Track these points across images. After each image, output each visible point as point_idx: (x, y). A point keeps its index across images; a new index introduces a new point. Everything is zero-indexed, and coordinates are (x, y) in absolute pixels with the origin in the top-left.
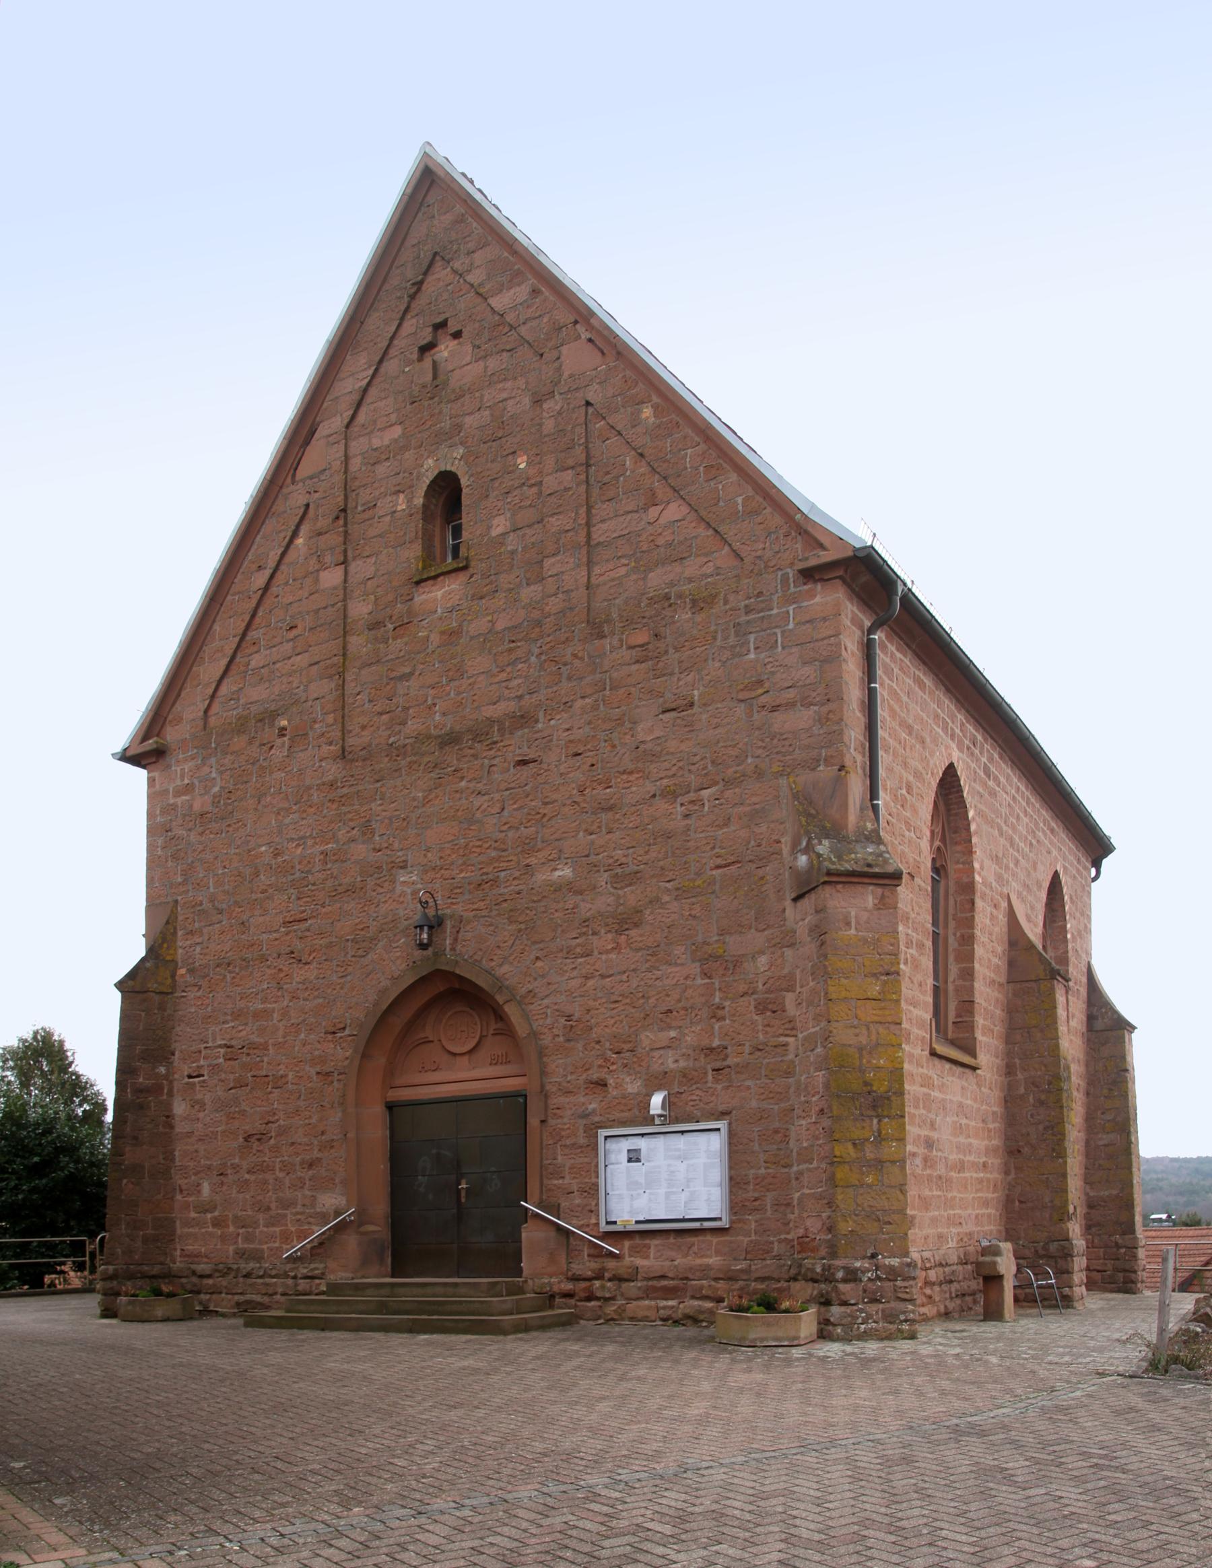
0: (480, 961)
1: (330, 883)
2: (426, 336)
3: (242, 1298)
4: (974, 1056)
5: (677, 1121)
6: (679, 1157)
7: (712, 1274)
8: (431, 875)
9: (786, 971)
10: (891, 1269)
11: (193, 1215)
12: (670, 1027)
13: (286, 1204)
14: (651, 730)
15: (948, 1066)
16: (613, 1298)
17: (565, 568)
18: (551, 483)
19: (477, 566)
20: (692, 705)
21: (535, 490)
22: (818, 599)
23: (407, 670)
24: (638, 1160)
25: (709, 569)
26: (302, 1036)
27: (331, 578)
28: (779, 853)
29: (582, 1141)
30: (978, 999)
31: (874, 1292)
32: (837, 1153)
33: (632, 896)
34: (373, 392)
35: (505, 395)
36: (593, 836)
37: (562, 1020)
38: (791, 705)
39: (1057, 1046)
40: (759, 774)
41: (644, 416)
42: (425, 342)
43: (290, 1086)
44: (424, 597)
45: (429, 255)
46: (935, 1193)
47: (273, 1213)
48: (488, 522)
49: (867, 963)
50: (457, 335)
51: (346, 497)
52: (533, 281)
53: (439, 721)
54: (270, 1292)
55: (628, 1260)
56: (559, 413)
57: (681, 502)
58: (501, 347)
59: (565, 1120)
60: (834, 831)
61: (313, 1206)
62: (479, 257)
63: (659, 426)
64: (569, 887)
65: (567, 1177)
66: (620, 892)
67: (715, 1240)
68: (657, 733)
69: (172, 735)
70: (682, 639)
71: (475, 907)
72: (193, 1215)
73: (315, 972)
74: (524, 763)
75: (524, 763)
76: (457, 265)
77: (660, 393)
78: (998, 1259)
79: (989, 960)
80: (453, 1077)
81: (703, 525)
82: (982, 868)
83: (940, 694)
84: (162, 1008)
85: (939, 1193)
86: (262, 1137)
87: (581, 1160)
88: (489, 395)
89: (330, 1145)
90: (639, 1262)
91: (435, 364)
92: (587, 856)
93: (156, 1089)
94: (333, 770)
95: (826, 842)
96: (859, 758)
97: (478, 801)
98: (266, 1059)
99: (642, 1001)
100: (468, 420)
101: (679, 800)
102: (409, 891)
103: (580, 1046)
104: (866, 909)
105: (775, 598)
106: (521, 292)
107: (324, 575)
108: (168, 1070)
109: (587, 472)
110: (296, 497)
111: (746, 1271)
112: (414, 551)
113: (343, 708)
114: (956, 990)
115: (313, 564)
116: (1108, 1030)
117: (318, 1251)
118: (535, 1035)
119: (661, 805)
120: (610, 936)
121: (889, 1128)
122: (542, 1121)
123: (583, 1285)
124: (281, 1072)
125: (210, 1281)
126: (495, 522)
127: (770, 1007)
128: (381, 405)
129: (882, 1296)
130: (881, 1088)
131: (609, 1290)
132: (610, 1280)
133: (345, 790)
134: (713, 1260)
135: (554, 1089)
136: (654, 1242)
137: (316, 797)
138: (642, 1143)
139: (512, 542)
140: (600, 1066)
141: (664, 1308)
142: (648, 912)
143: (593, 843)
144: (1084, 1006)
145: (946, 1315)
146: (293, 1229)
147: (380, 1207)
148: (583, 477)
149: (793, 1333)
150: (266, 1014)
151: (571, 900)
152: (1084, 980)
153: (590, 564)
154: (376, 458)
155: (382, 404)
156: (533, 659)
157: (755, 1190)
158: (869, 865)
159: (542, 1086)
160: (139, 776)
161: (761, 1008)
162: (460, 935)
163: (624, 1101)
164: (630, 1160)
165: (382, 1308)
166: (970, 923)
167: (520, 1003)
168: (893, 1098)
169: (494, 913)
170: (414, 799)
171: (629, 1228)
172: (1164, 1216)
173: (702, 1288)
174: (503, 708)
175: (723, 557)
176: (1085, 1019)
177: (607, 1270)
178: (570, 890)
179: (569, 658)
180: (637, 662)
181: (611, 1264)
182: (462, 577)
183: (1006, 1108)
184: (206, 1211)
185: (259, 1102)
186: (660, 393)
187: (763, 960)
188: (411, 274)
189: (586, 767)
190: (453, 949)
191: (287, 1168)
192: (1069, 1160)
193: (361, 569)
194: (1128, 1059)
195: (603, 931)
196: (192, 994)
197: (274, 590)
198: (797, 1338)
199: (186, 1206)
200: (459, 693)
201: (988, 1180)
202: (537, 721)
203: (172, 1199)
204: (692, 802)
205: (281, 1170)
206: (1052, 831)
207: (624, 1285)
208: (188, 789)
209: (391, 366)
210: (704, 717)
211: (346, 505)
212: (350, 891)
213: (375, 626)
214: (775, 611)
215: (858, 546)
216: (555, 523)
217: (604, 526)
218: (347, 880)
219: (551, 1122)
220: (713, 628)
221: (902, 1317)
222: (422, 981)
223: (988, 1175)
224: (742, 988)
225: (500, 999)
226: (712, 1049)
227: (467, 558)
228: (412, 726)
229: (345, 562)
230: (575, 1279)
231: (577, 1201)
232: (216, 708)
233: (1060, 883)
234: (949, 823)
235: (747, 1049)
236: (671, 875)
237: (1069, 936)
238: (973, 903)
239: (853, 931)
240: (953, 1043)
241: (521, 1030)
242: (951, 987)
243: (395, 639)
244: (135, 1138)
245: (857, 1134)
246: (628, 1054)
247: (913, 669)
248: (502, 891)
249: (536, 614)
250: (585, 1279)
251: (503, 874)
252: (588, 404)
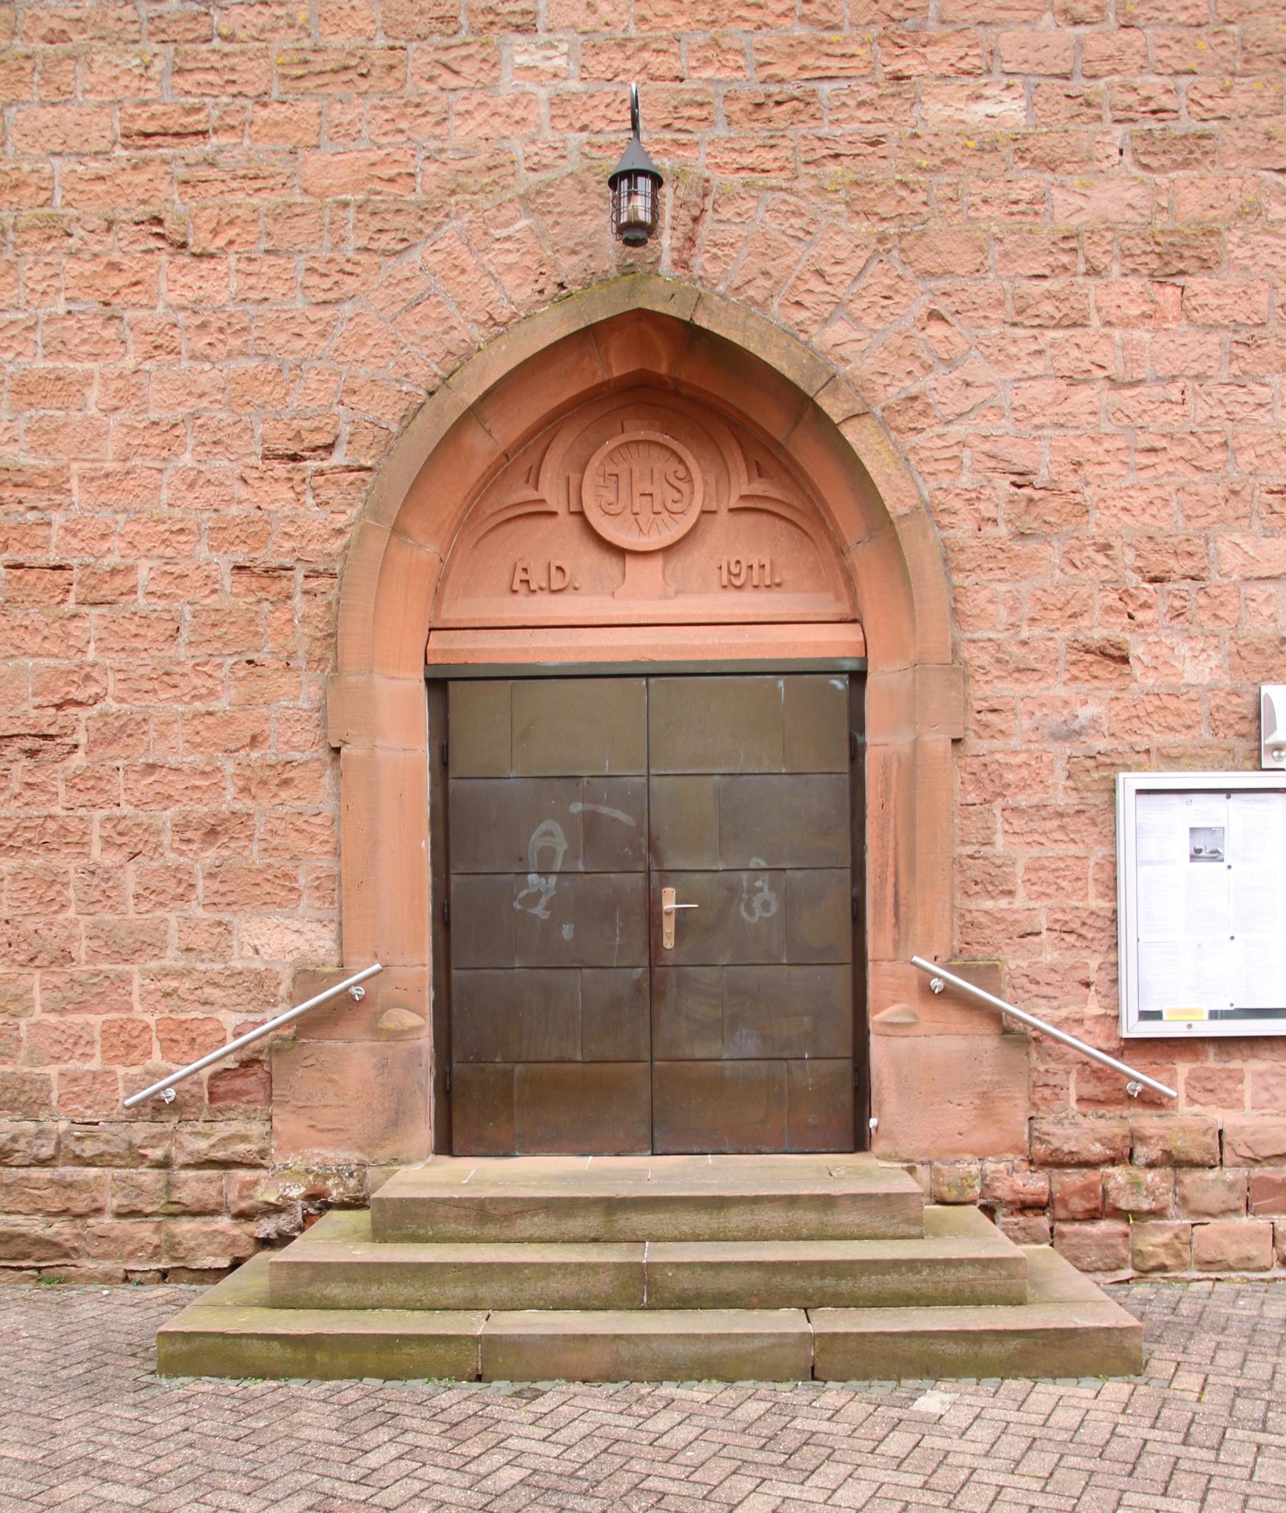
0: (763, 305)
1: (283, 41)
24: (1215, 856)
26: (187, 459)
33: (1192, 195)
36: (1081, 30)
37: (1004, 483)
43: (142, 602)
47: (80, 969)
54: (80, 1207)
59: (1014, 743)
61: (220, 952)
65: (1021, 892)
66: (1159, 178)
71: (746, 160)
73: (235, 283)
87: (1061, 849)
89: (282, 777)
92: (1066, 77)
98: (58, 518)
99: (1219, 456)
102: (543, 94)
103: (1053, 553)
117: (238, 1084)
120: (1135, 284)
122: (956, 742)
123: (1074, 1178)
124: (112, 560)
131: (1151, 1192)
132: (1151, 1165)
135: (985, 660)
136: (1254, 1066)
140: (1109, 610)
142: (1234, 237)
143: (1080, 45)
146: (151, 1020)
151: (1028, 182)
162: (704, 230)
163: (1173, 704)
164: (1196, 855)
167: (884, 424)
169: (803, 185)
177: (1143, 1140)
178: (1021, 154)
185: (33, 643)
191: (129, 840)
195: (1116, 269)
205: (108, 842)
207: (1191, 1178)
212: (352, 69)
219: (975, 745)
222: (588, 338)
225: (834, 408)
230: (1056, 1162)
231: (1050, 957)
241: (895, 499)
246: (1185, 584)
251: (826, 88)
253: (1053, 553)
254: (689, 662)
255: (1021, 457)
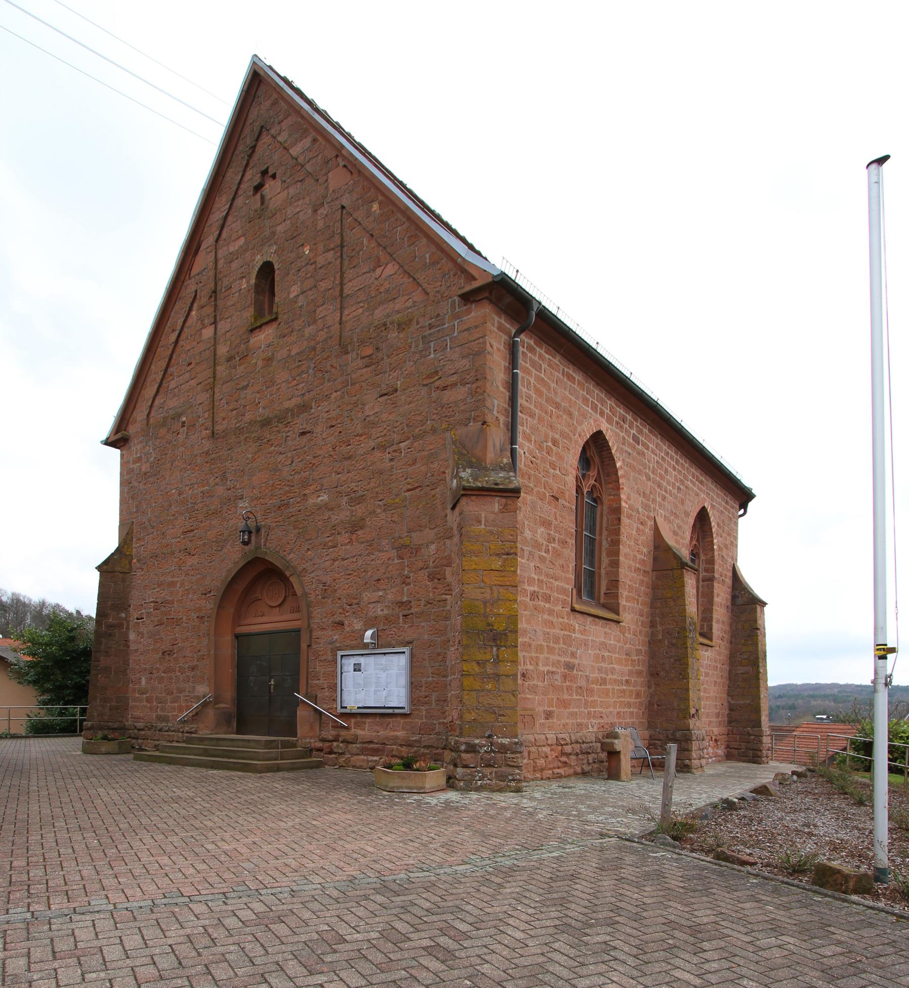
1: (205, 509)
2: (257, 180)
3: (157, 742)
4: (618, 614)
5: (382, 647)
6: (382, 669)
7: (399, 742)
8: (255, 502)
9: (446, 554)
10: (502, 745)
11: (137, 695)
12: (379, 590)
13: (180, 691)
14: (373, 408)
15: (590, 619)
16: (343, 753)
17: (328, 313)
18: (321, 260)
19: (282, 318)
20: (396, 390)
21: (313, 266)
22: (473, 314)
23: (245, 384)
24: (360, 670)
25: (409, 304)
27: (208, 332)
28: (444, 480)
29: (330, 658)
30: (622, 578)
31: (489, 760)
32: (465, 669)
33: (360, 510)
34: (230, 218)
35: (298, 210)
37: (321, 586)
38: (454, 385)
39: (685, 610)
40: (434, 430)
41: (374, 209)
42: (256, 184)
44: (255, 339)
45: (259, 128)
46: (575, 697)
48: (289, 290)
49: (492, 547)
50: (274, 177)
51: (216, 284)
52: (313, 134)
53: (262, 412)
55: (353, 731)
56: (326, 216)
57: (394, 262)
58: (297, 179)
60: (478, 465)
62: (284, 125)
63: (382, 215)
64: (327, 507)
66: (354, 508)
67: (402, 721)
68: (377, 410)
69: (132, 430)
70: (391, 350)
72: (137, 695)
74: (303, 434)
75: (303, 434)
76: (273, 132)
77: (383, 194)
78: (616, 741)
79: (635, 556)
80: (273, 619)
81: (407, 275)
82: (629, 498)
83: (591, 386)
84: (124, 581)
85: (579, 697)
86: (170, 653)
88: (290, 211)
90: (360, 732)
91: (262, 197)
93: (120, 626)
94: (207, 445)
95: (469, 471)
96: (502, 419)
97: (280, 458)
100: (279, 228)
101: (388, 450)
103: (329, 601)
104: (493, 512)
105: (447, 317)
106: (307, 142)
107: (204, 331)
108: (126, 615)
109: (342, 251)
110: (190, 287)
111: (419, 741)
112: (249, 313)
113: (213, 408)
114: (607, 574)
115: (199, 325)
116: (746, 606)
118: (306, 594)
119: (378, 454)
121: (505, 653)
123: (328, 744)
125: (143, 733)
126: (292, 289)
127: (436, 576)
128: (235, 225)
129: (495, 763)
130: (500, 626)
132: (342, 742)
133: (213, 456)
134: (400, 734)
137: (199, 460)
138: (362, 660)
139: (301, 301)
141: (371, 761)
143: (339, 479)
144: (729, 590)
145: (584, 774)
147: (229, 693)
148: (339, 254)
149: (420, 785)
150: (173, 584)
152: (730, 574)
153: (342, 309)
154: (232, 257)
155: (234, 225)
156: (311, 371)
157: (425, 691)
158: (497, 484)
159: (309, 625)
160: (117, 452)
161: (431, 577)
165: (206, 753)
166: (617, 532)
167: (299, 576)
168: (509, 634)
170: (247, 459)
171: (353, 711)
172: (825, 717)
173: (393, 750)
174: (294, 401)
175: (418, 296)
176: (730, 597)
179: (329, 368)
180: (366, 366)
181: (343, 733)
182: (275, 325)
183: (650, 647)
184: (143, 693)
186: (383, 194)
187: (433, 547)
188: (249, 141)
189: (337, 433)
190: (265, 545)
192: (691, 681)
193: (223, 326)
194: (759, 622)
196: (139, 573)
197: (181, 343)
198: (424, 788)
199: (134, 690)
200: (272, 395)
201: (631, 691)
202: (311, 408)
203: (127, 686)
204: (394, 451)
206: (701, 482)
207: (350, 746)
208: (139, 460)
209: (239, 202)
210: (403, 397)
211: (216, 288)
212: (215, 513)
213: (230, 359)
214: (446, 326)
215: (495, 274)
216: (323, 285)
217: (350, 284)
218: (213, 507)
219: (314, 646)
220: (410, 340)
221: (510, 778)
223: (632, 688)
224: (420, 565)
225: (287, 574)
226: (402, 603)
227: (277, 313)
228: (248, 417)
229: (215, 323)
230: (323, 740)
232: (153, 413)
233: (708, 514)
234: (603, 470)
235: (423, 603)
236: (381, 497)
237: (715, 547)
238: (619, 519)
239: (483, 526)
240: (604, 606)
241: (299, 592)
242: (603, 572)
243: (240, 365)
244: (107, 652)
245: (480, 657)
247: (562, 367)
248: (291, 510)
249: (312, 343)
250: (329, 741)
252: (343, 207)
253: (329, 601)
254: (885, 593)
255: (324, 579)
